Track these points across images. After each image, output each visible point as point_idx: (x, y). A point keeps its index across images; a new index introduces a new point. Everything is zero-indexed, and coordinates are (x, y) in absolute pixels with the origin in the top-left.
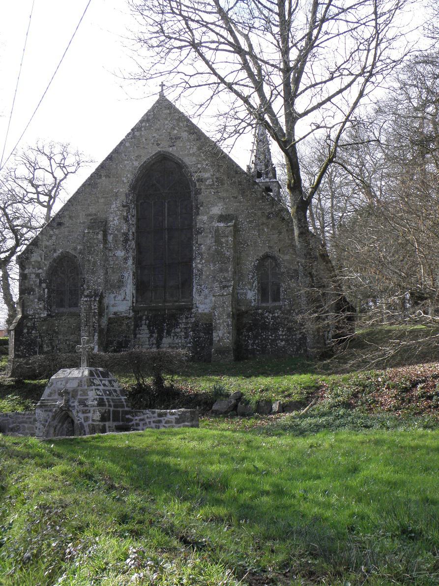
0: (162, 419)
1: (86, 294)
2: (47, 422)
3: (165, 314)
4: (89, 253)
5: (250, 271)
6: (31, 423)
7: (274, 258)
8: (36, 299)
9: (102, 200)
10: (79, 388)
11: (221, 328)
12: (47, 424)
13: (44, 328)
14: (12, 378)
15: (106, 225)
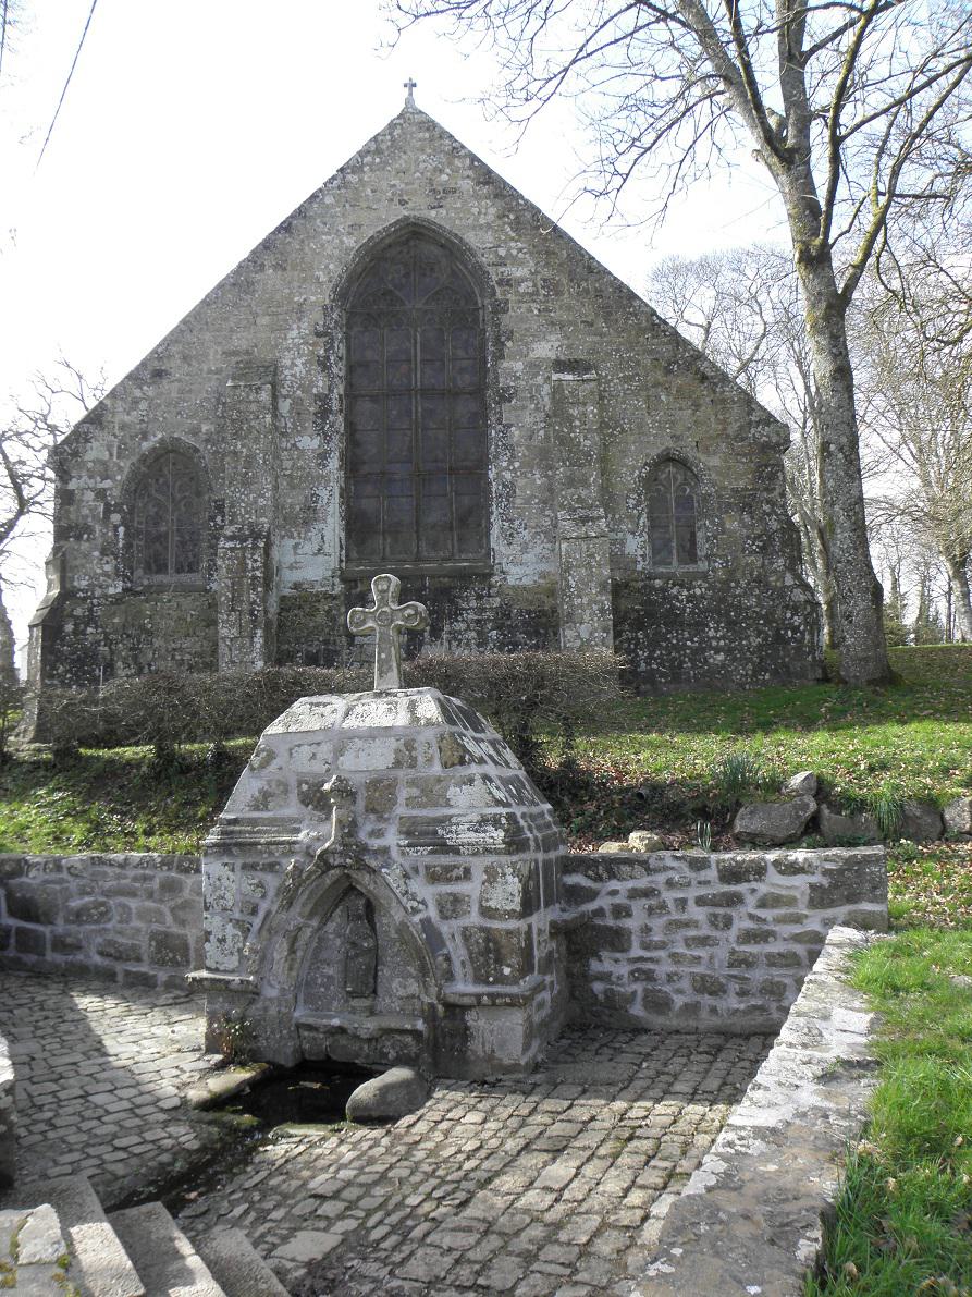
0: (742, 888)
1: (229, 533)
2: (254, 912)
3: (424, 588)
4: (237, 435)
5: (630, 490)
6: (150, 895)
7: (682, 463)
8: (95, 549)
9: (265, 320)
10: (400, 773)
11: (586, 618)
12: (257, 921)
13: (116, 620)
14: (37, 744)
15: (275, 374)
